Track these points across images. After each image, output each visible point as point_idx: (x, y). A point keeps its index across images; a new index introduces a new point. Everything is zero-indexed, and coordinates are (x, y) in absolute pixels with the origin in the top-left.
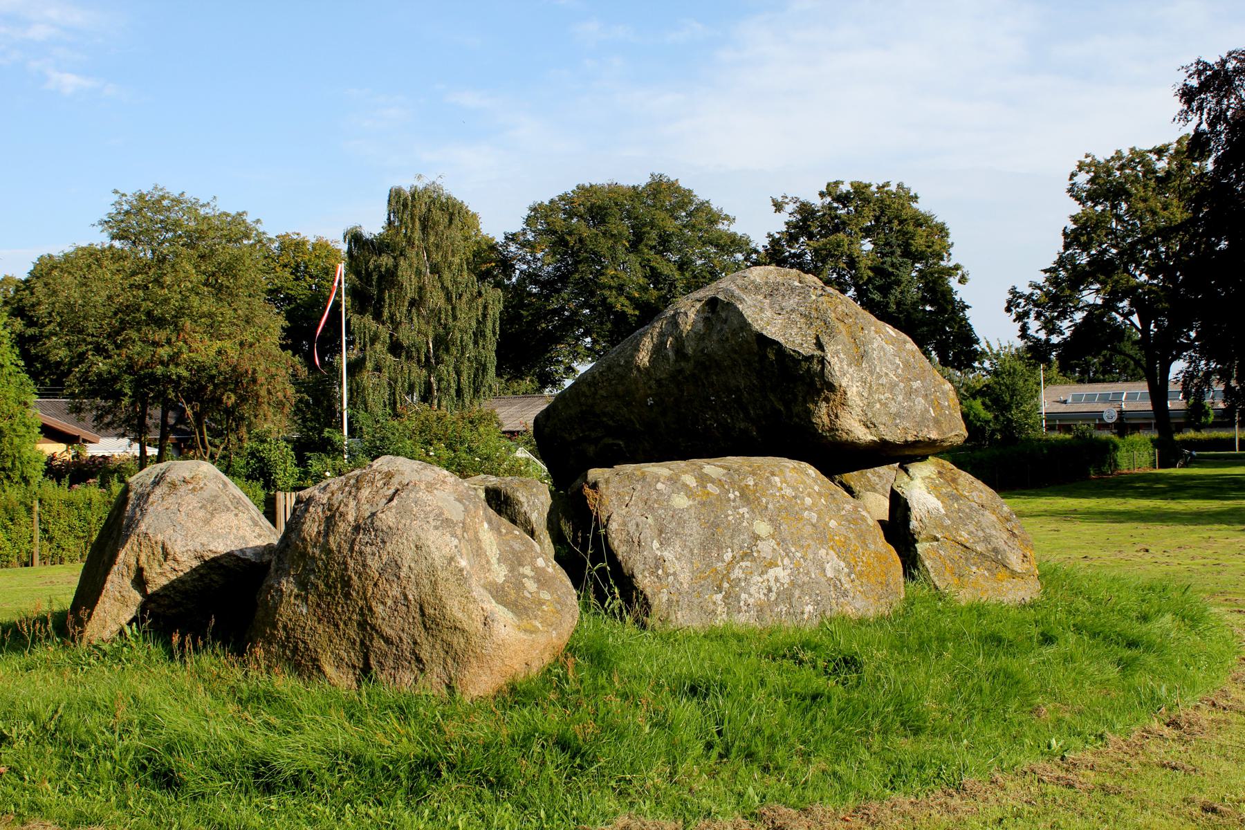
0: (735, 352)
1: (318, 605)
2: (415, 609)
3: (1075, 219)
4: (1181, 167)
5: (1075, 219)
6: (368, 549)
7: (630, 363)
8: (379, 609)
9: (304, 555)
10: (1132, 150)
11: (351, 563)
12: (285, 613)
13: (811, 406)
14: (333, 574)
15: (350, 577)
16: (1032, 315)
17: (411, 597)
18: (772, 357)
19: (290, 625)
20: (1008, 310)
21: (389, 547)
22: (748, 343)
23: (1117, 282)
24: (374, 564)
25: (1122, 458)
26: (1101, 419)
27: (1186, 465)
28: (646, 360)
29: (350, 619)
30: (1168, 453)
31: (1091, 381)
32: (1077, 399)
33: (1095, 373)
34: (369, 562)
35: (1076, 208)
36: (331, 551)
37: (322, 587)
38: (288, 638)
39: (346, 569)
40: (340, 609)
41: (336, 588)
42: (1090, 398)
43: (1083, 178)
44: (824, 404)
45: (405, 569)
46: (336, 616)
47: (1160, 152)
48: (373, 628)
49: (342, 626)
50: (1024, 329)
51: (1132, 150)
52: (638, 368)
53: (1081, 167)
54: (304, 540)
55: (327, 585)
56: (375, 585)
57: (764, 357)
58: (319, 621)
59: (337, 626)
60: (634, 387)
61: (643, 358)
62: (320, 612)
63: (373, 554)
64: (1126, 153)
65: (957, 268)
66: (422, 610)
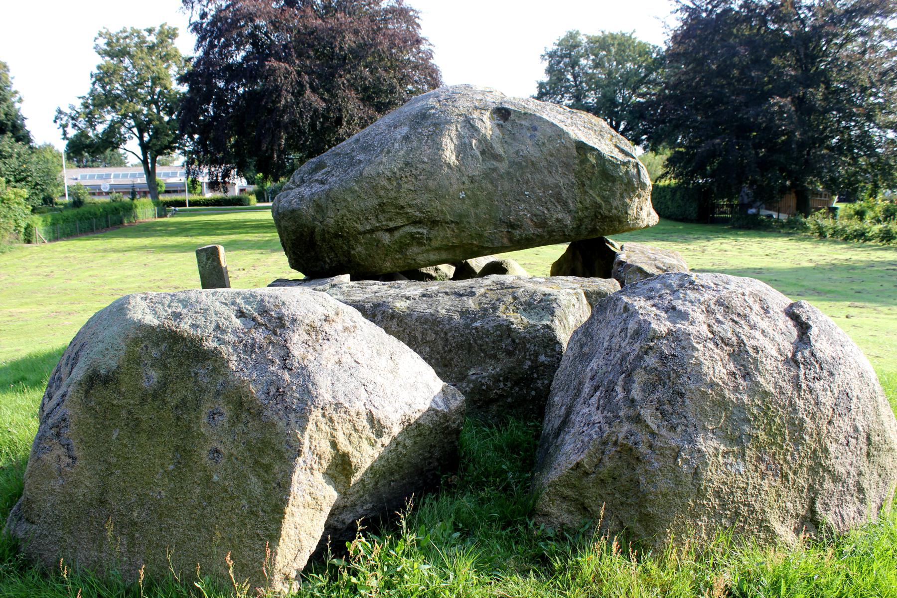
0: (552, 155)
1: (760, 459)
2: (862, 438)
3: (99, 67)
4: (162, 42)
5: (99, 67)
6: (818, 385)
7: (436, 160)
8: (832, 448)
9: (722, 404)
10: (132, 28)
11: (800, 403)
12: (713, 476)
13: (627, 200)
14: (777, 420)
15: (802, 421)
16: (70, 125)
17: (861, 429)
18: (593, 161)
19: (725, 489)
20: (55, 122)
21: (838, 379)
22: (567, 148)
23: (127, 107)
24: (827, 400)
25: (139, 212)
26: (100, 189)
27: (173, 216)
28: (454, 158)
29: (801, 466)
30: (163, 208)
31: (85, 166)
32: (84, 177)
33: (87, 161)
34: (822, 399)
35: (101, 61)
36: (766, 393)
37: (762, 436)
38: (723, 505)
39: (795, 411)
40: (789, 458)
41: (783, 435)
42: (92, 177)
43: (102, 42)
44: (637, 200)
45: (854, 399)
46: (785, 467)
47: (150, 31)
48: (826, 470)
49: (791, 476)
50: (65, 133)
51: (132, 28)
52: (449, 165)
53: (100, 35)
54: (712, 385)
55: (769, 434)
56: (830, 422)
57: (584, 161)
58: (763, 476)
59: (785, 477)
60: (446, 182)
61: (450, 155)
62: (763, 467)
63: (825, 390)
64: (129, 30)
65: (16, 92)
66: (868, 438)
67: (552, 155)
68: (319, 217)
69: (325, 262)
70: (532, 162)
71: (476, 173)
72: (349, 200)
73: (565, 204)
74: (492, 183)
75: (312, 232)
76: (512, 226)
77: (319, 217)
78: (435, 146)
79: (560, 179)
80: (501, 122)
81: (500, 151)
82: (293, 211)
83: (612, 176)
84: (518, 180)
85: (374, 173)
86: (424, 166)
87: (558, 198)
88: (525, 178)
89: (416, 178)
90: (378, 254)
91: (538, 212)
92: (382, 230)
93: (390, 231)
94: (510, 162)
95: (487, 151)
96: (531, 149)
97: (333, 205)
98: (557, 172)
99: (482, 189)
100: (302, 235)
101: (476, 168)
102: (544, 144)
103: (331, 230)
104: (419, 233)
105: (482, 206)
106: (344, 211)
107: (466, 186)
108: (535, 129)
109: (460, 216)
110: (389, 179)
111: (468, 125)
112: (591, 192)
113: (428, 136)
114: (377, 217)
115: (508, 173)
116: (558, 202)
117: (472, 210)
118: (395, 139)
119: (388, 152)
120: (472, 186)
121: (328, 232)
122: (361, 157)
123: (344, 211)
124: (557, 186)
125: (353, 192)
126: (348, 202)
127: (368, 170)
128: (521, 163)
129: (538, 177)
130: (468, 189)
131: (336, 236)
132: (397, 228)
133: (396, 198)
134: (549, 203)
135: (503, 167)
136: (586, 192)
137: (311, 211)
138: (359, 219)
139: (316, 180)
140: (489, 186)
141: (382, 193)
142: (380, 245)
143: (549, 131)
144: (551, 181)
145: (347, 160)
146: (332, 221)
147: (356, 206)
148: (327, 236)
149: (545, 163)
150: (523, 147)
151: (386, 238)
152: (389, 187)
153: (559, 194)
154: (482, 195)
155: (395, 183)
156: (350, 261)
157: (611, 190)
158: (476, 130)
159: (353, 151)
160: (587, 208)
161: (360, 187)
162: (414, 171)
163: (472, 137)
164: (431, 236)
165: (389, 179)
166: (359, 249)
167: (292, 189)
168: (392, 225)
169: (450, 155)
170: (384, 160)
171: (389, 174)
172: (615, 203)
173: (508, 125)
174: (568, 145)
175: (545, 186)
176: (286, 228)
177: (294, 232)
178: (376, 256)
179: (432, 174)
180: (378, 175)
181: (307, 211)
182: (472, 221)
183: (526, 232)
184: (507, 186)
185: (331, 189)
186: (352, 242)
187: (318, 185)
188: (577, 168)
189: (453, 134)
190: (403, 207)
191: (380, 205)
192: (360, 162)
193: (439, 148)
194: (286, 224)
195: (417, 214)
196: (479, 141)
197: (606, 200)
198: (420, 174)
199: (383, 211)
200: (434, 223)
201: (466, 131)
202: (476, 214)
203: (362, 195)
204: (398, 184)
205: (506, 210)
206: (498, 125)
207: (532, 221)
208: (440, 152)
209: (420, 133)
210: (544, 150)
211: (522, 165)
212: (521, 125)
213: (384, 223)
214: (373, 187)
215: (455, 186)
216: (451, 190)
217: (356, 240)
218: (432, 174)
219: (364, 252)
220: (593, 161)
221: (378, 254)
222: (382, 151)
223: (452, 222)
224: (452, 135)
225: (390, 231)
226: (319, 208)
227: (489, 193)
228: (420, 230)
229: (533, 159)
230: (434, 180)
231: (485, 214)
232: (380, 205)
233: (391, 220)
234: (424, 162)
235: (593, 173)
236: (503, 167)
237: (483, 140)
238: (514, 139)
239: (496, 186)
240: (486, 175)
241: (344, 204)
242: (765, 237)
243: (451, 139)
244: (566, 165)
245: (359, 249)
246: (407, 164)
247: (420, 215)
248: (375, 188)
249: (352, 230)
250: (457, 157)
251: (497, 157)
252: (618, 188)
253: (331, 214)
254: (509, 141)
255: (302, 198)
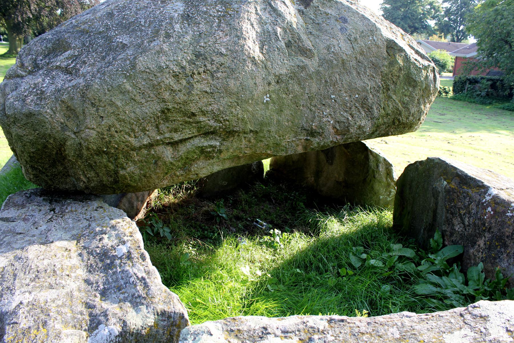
7: (237, 52)
18: (401, 62)
22: (378, 47)
28: (257, 49)
60: (251, 82)
61: (253, 47)
67: (362, 53)
68: (72, 125)
69: (78, 179)
70: (343, 60)
71: (284, 71)
72: (119, 104)
73: (369, 110)
74: (300, 84)
75: (61, 145)
76: (312, 133)
77: (72, 125)
78: (234, 33)
79: (367, 82)
80: (302, 8)
81: (308, 44)
82: (30, 115)
83: (415, 81)
84: (326, 82)
85: (153, 67)
86: (222, 60)
87: (364, 103)
88: (334, 79)
89: (213, 76)
90: (156, 173)
91: (342, 119)
92: (163, 143)
93: (174, 144)
94: (320, 60)
95: (294, 45)
96: (342, 44)
97: (93, 110)
98: (365, 73)
99: (287, 92)
100: (45, 147)
101: (283, 66)
102: (356, 39)
103: (91, 146)
104: (211, 146)
105: (287, 112)
106: (112, 120)
107: (272, 88)
108: (345, 21)
109: (262, 124)
110: (176, 76)
111: (269, 9)
112: (394, 97)
113: (219, 17)
114: (157, 127)
115: (318, 73)
116: (362, 107)
117: (275, 117)
118: (172, 18)
119: (168, 36)
120: (277, 87)
121: (88, 149)
122: (125, 39)
123: (112, 120)
124: (364, 90)
125: (124, 92)
126: (117, 107)
127: (144, 62)
128: (332, 62)
129: (346, 78)
130: (274, 91)
131: (99, 152)
132: (182, 141)
133: (185, 103)
134: (353, 108)
135: (312, 64)
136: (390, 97)
137: (60, 117)
138: (133, 130)
139: (58, 67)
140: (296, 88)
141: (167, 95)
142: (160, 163)
143: (361, 26)
144: (359, 84)
145: (101, 41)
146: (93, 134)
147: (130, 112)
148: (85, 152)
149: (354, 63)
150: (335, 42)
151: (168, 154)
152: (176, 87)
153: (366, 98)
154: (287, 99)
155: (184, 82)
156: (116, 182)
157: (410, 96)
158: (279, 15)
159: (108, 29)
160: (388, 115)
161: (134, 86)
162: (209, 67)
163: (275, 23)
164: (223, 148)
165: (176, 76)
166: (131, 168)
167: (22, 77)
168: (177, 137)
169: (253, 47)
170: (165, 47)
171: (176, 69)
172: (413, 110)
173: (310, 12)
174: (380, 43)
175: (352, 90)
176: (20, 138)
177: (33, 143)
178: (153, 176)
179: (233, 71)
180: (161, 69)
181: (53, 117)
182: (273, 129)
183: (326, 141)
184: (314, 87)
185: (88, 86)
186: (122, 160)
187: (63, 76)
188: (385, 70)
189: (253, 17)
190: (193, 114)
191: (163, 112)
192: (124, 46)
193: (239, 35)
194: (20, 132)
195: (212, 123)
196: (284, 30)
197: (405, 105)
198: (216, 72)
199: (167, 120)
200: (230, 133)
201: (268, 16)
202: (278, 121)
203: (138, 98)
204: (189, 83)
205: (310, 117)
206: (299, 11)
207: (334, 128)
208: (242, 42)
209: (205, 13)
210: (356, 47)
211: (334, 64)
212: (327, 14)
213: (167, 135)
214: (154, 86)
215: (260, 88)
216: (255, 93)
217: (128, 157)
218: (233, 71)
219: (137, 172)
220: (401, 62)
221: (156, 173)
222: (156, 33)
223: (251, 131)
224: (252, 20)
225: (174, 144)
226: (70, 111)
227: (295, 97)
228: (213, 143)
229: (345, 57)
230: (237, 79)
231: (288, 121)
232: (163, 112)
233: (176, 131)
234: (222, 54)
235: (399, 77)
236: (312, 64)
237: (288, 29)
238: (320, 30)
239: (303, 88)
240: (293, 76)
241: (110, 109)
242: (477, 129)
243: (252, 25)
244: (375, 66)
245: (131, 168)
246: (198, 55)
247: (215, 124)
248: (156, 88)
249: (123, 145)
250: (261, 49)
251: (305, 52)
252: (417, 93)
253: (91, 122)
254: (314, 32)
255: (41, 95)
